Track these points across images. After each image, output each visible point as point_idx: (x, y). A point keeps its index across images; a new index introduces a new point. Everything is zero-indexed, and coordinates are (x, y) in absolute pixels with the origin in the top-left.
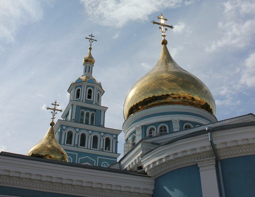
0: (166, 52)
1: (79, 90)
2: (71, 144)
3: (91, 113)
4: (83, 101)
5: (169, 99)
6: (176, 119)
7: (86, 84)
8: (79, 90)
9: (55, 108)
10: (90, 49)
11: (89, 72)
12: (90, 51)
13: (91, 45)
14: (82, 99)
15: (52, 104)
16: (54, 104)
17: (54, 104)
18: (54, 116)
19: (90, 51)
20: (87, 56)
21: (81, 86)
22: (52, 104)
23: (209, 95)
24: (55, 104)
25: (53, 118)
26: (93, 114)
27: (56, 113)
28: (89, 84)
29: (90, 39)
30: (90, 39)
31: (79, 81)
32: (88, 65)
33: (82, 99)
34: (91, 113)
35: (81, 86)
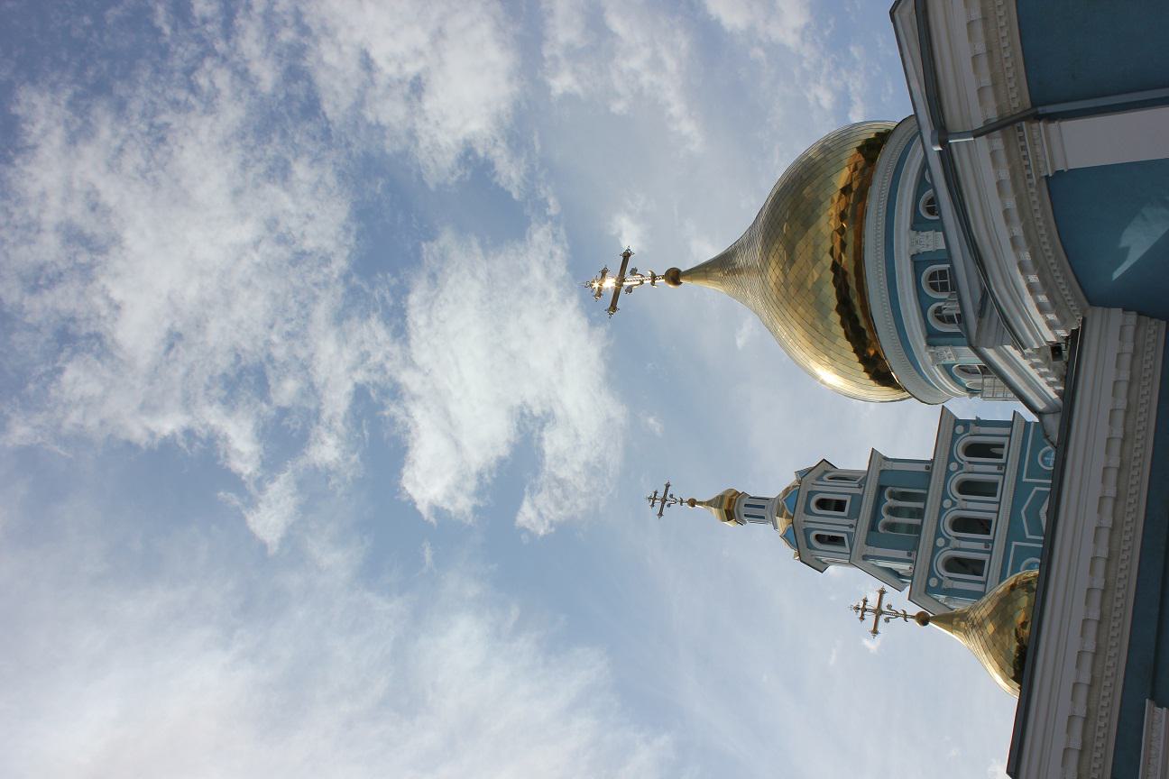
0: (703, 271)
1: (818, 537)
2: (846, 501)
3: (890, 502)
4: (851, 526)
5: (847, 262)
6: (906, 243)
7: (800, 516)
8: (818, 537)
9: (874, 611)
10: (693, 503)
12: (701, 503)
14: (847, 529)
15: (862, 618)
16: (863, 615)
17: (863, 615)
18: (897, 615)
19: (701, 503)
21: (807, 532)
24: (860, 612)
25: (905, 616)
26: (893, 496)
27: (889, 607)
28: (801, 506)
29: (663, 503)
30: (663, 503)
31: (792, 537)
32: (743, 510)
33: (847, 529)
34: (890, 502)
35: (807, 532)
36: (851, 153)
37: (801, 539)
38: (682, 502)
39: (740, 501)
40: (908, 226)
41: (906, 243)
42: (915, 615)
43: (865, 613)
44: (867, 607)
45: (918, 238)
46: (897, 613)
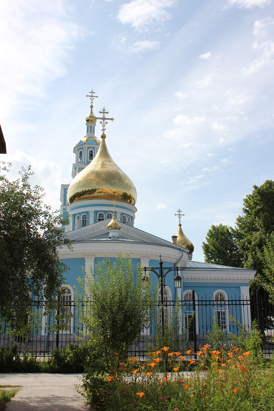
1: (81, 152)
4: (84, 162)
5: (95, 194)
6: (91, 210)
7: (86, 146)
8: (81, 152)
9: (104, 117)
10: (92, 107)
11: (91, 132)
12: (92, 110)
13: (92, 103)
14: (84, 161)
15: (100, 112)
19: (92, 110)
20: (88, 115)
21: (82, 148)
22: (100, 112)
23: (127, 182)
24: (103, 111)
25: (103, 130)
27: (107, 123)
28: (90, 146)
29: (91, 96)
30: (91, 96)
31: (81, 144)
32: (90, 125)
33: (84, 161)
35: (82, 148)
36: (121, 191)
37: (80, 147)
38: (92, 103)
39: (92, 123)
40: (95, 210)
41: (91, 210)
42: (105, 134)
43: (103, 113)
44: (105, 114)
45: (93, 212)
46: (105, 126)
